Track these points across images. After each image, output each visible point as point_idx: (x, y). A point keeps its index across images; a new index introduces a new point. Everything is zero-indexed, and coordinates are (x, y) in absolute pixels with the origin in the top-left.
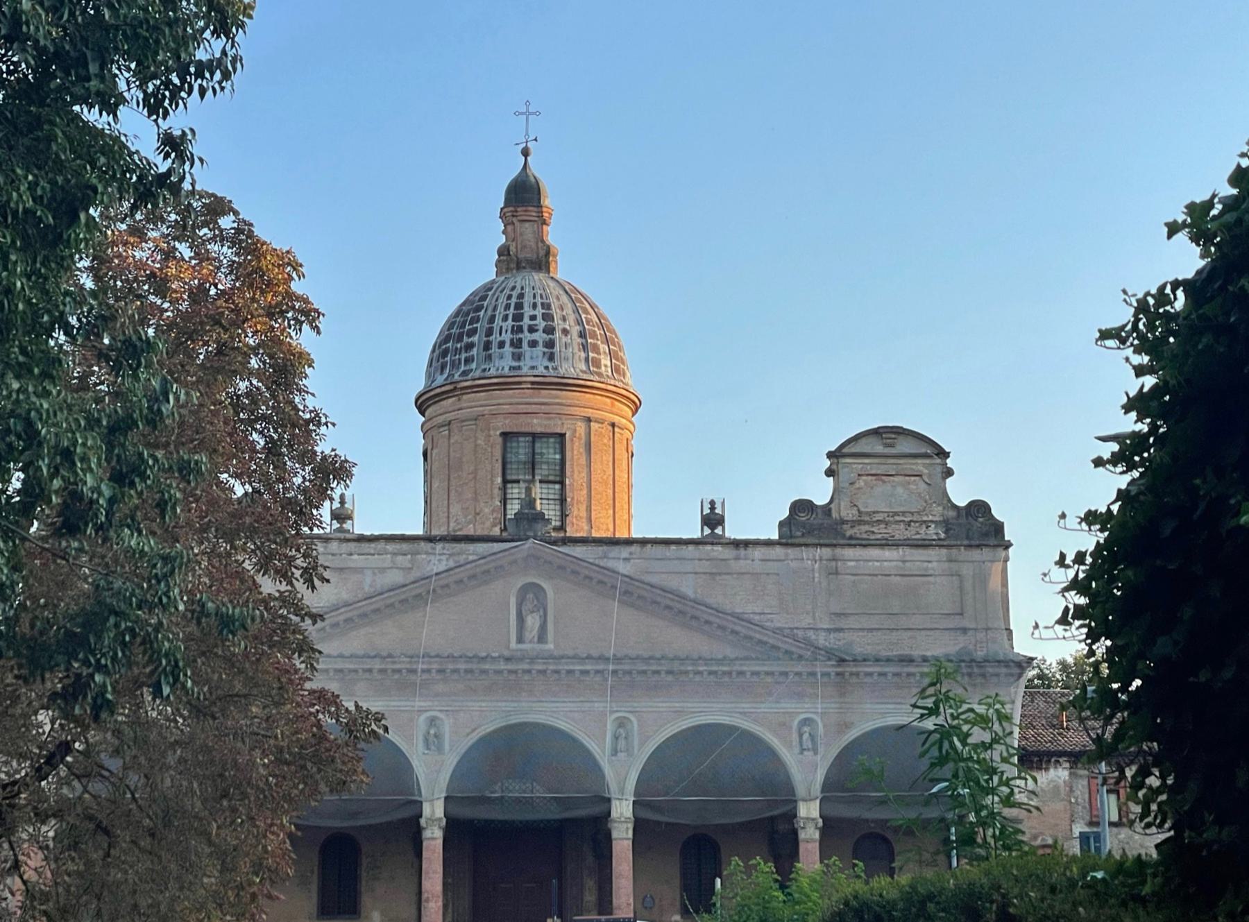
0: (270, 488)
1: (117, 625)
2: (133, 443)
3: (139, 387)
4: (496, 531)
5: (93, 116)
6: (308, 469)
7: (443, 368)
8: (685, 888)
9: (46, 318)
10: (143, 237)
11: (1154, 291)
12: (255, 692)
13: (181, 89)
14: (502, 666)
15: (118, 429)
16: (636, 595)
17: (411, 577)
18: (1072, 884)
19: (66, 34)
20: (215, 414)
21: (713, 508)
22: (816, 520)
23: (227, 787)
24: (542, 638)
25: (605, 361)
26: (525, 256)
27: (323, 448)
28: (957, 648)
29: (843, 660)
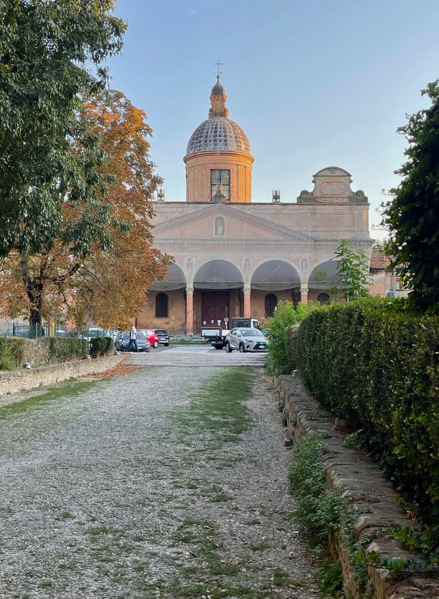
0: (138, 187)
1: (89, 228)
2: (94, 170)
3: (94, 153)
4: (209, 201)
5: (76, 63)
6: (149, 180)
7: (192, 148)
8: (266, 310)
9: (64, 130)
10: (96, 106)
11: (416, 114)
12: (134, 249)
13: (104, 53)
14: (211, 242)
15: (88, 166)
16: (252, 221)
17: (183, 214)
18: (381, 306)
19: (68, 36)
20: (120, 162)
21: (276, 193)
22: (309, 196)
23: (126, 279)
24: (223, 234)
25: (243, 146)
26: (219, 112)
27: (154, 174)
28: (352, 237)
29: (316, 241)
